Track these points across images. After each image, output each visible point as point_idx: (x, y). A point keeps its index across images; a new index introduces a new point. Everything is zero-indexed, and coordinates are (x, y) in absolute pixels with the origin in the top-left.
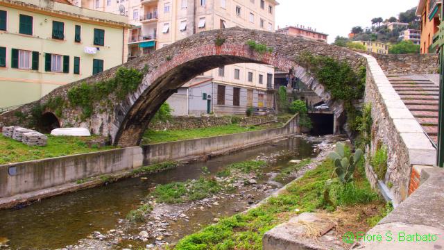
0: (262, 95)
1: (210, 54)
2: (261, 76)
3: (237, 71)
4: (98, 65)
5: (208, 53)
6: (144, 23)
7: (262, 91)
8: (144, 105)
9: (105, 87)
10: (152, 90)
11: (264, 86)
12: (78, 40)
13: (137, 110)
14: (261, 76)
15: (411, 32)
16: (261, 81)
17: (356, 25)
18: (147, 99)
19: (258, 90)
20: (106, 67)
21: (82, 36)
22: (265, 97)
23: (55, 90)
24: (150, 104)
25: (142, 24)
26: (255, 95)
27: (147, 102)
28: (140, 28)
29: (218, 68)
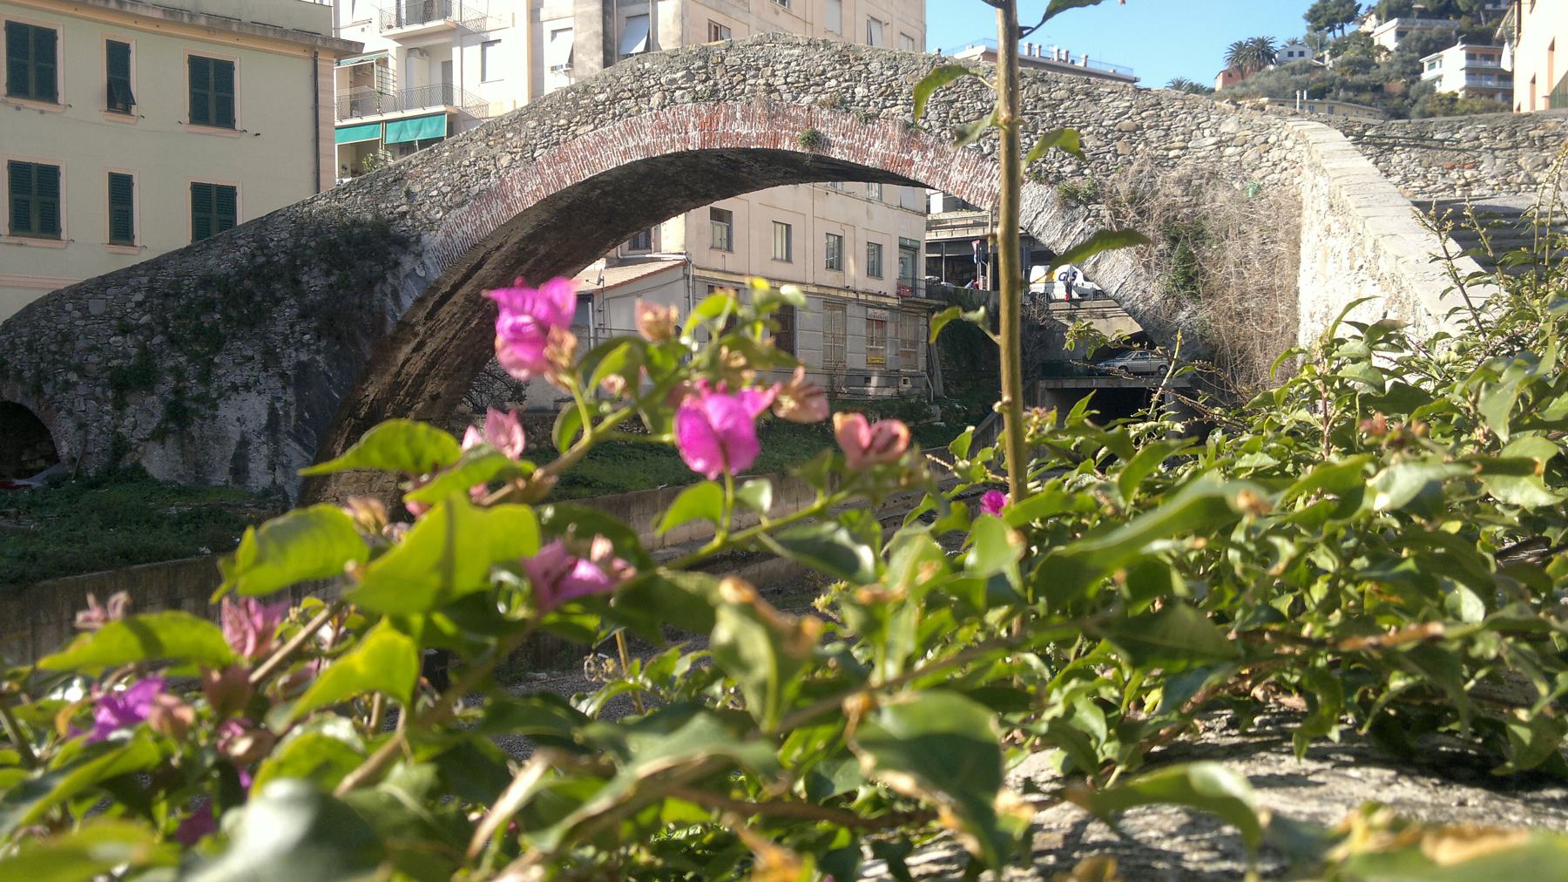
0: (881, 323)
1: (678, 147)
2: (875, 250)
3: (122, 229)
4: (1054, 243)
5: (670, 145)
6: (399, 39)
7: (880, 306)
8: (418, 364)
9: (1396, 67)
10: (446, 298)
11: (888, 283)
12: (119, 96)
13: (387, 379)
14: (875, 250)
15: (1470, 57)
16: (875, 270)
17: (1245, 35)
18: (432, 333)
19: (868, 305)
20: (246, 212)
21: (139, 80)
22: (890, 329)
23: (30, 308)
24: (438, 355)
25: (392, 47)
26: (856, 323)
27: (428, 349)
28: (383, 62)
29: (682, 217)
